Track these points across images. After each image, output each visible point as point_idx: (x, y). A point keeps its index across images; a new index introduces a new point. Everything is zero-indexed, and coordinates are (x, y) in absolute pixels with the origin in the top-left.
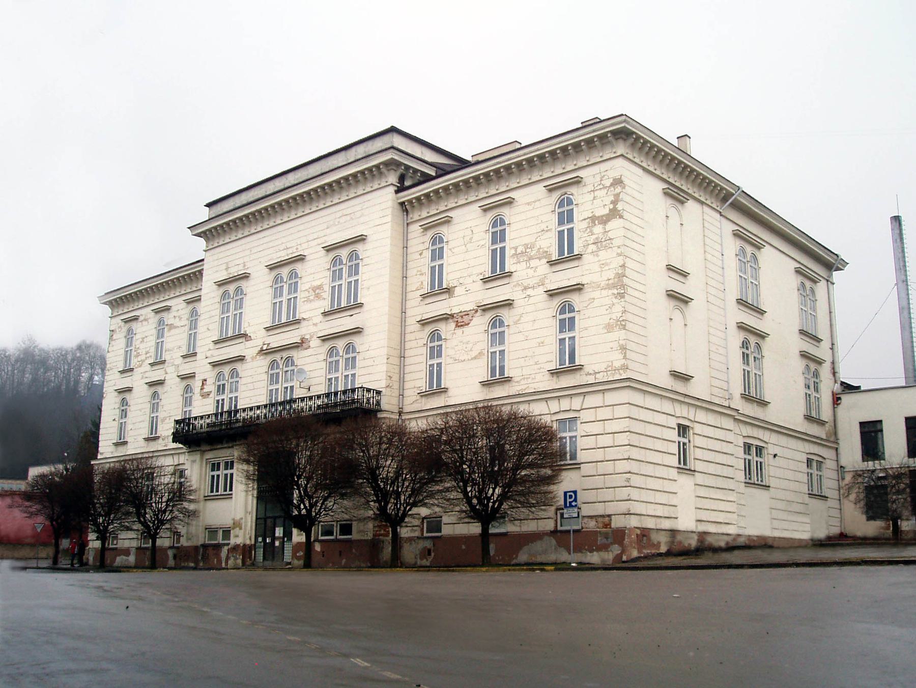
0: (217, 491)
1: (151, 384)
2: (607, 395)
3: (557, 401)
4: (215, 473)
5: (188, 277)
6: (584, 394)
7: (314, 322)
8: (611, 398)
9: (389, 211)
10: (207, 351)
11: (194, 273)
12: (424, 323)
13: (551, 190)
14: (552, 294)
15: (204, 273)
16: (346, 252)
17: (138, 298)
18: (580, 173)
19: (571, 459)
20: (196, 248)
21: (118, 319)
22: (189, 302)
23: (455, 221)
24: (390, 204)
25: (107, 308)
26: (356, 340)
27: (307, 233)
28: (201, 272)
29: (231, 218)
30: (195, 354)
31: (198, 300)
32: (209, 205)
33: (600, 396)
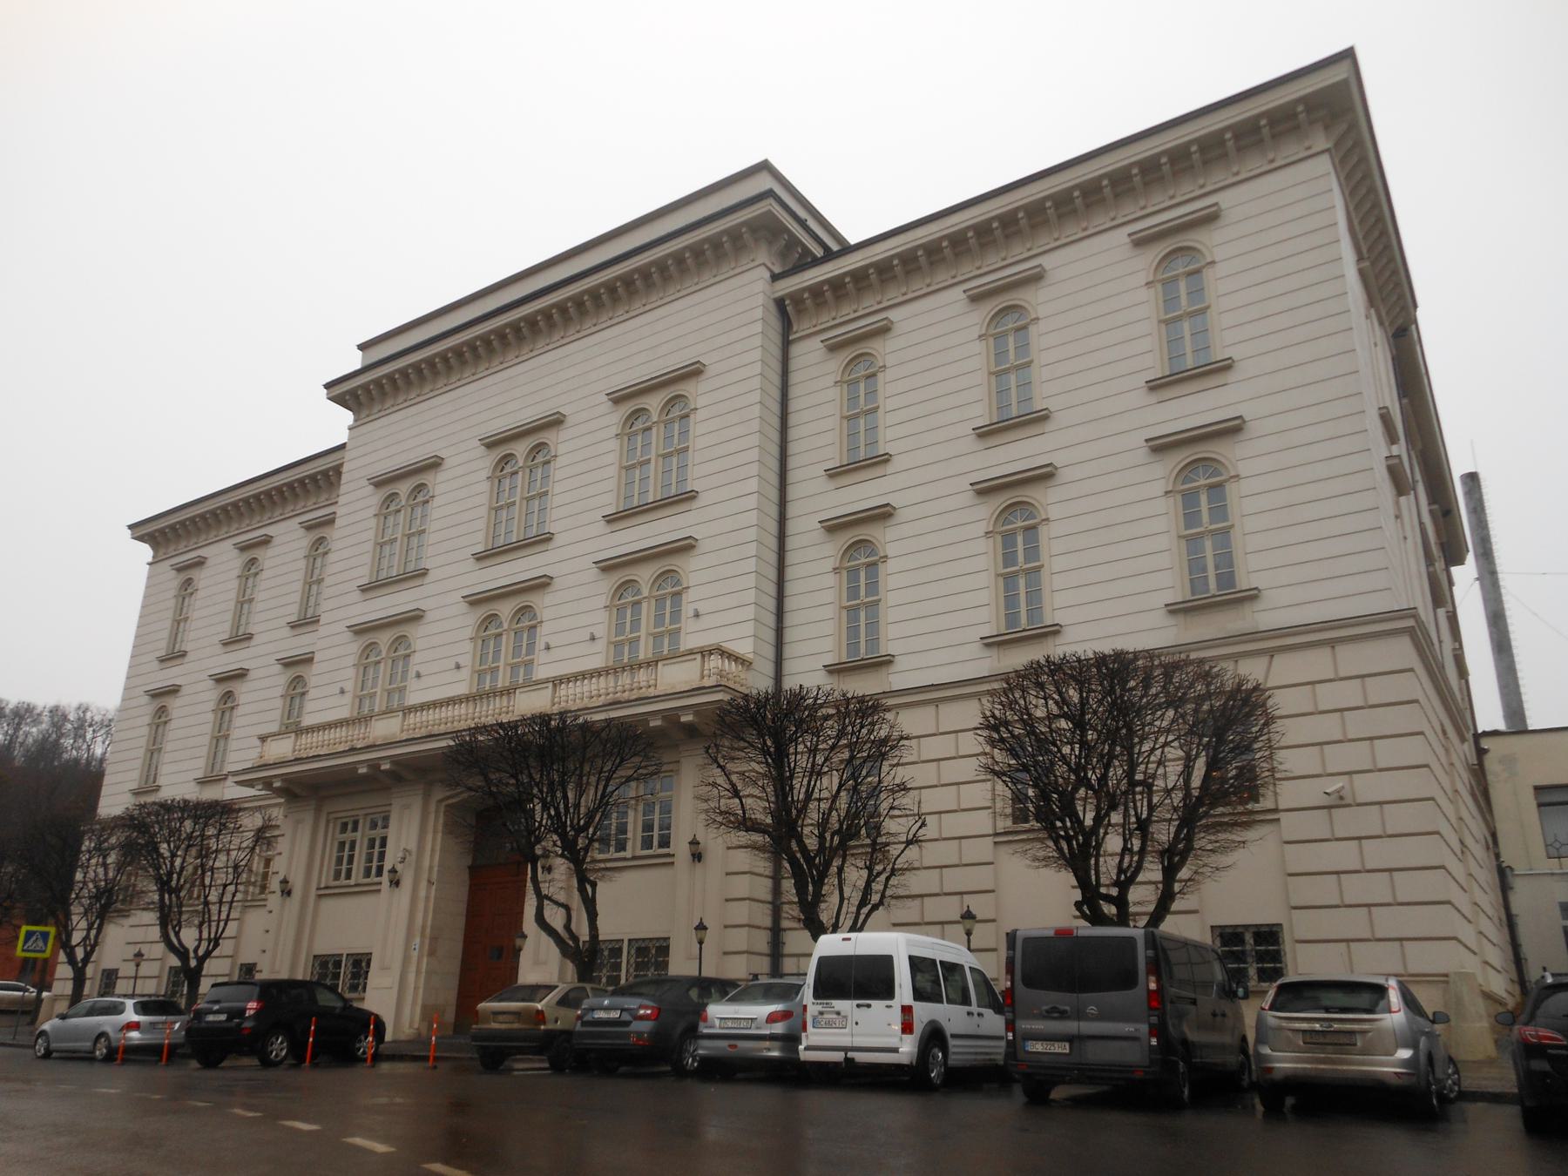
0: (348, 876)
1: (288, 663)
2: (1343, 651)
3: (1327, 651)
4: (349, 836)
5: (305, 486)
6: (1271, 653)
7: (452, 575)
8: (1354, 658)
9: (759, 313)
10: (345, 606)
11: (325, 473)
12: (834, 527)
13: (976, 298)
14: (985, 490)
15: (345, 469)
16: (656, 404)
17: (209, 526)
18: (893, 315)
19: (661, 846)
20: (336, 425)
21: (166, 565)
22: (244, 548)
23: (897, 329)
24: (760, 299)
25: (145, 551)
26: (539, 601)
27: (574, 377)
28: (338, 470)
29: (387, 378)
30: (315, 621)
31: (329, 521)
32: (363, 347)
33: (1324, 654)
